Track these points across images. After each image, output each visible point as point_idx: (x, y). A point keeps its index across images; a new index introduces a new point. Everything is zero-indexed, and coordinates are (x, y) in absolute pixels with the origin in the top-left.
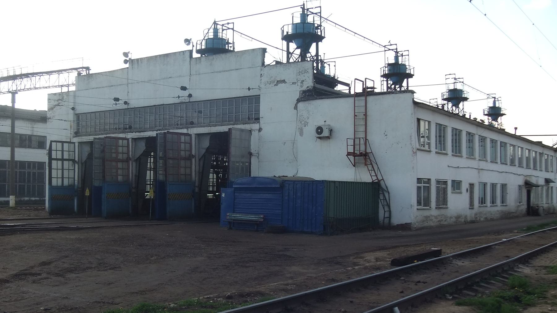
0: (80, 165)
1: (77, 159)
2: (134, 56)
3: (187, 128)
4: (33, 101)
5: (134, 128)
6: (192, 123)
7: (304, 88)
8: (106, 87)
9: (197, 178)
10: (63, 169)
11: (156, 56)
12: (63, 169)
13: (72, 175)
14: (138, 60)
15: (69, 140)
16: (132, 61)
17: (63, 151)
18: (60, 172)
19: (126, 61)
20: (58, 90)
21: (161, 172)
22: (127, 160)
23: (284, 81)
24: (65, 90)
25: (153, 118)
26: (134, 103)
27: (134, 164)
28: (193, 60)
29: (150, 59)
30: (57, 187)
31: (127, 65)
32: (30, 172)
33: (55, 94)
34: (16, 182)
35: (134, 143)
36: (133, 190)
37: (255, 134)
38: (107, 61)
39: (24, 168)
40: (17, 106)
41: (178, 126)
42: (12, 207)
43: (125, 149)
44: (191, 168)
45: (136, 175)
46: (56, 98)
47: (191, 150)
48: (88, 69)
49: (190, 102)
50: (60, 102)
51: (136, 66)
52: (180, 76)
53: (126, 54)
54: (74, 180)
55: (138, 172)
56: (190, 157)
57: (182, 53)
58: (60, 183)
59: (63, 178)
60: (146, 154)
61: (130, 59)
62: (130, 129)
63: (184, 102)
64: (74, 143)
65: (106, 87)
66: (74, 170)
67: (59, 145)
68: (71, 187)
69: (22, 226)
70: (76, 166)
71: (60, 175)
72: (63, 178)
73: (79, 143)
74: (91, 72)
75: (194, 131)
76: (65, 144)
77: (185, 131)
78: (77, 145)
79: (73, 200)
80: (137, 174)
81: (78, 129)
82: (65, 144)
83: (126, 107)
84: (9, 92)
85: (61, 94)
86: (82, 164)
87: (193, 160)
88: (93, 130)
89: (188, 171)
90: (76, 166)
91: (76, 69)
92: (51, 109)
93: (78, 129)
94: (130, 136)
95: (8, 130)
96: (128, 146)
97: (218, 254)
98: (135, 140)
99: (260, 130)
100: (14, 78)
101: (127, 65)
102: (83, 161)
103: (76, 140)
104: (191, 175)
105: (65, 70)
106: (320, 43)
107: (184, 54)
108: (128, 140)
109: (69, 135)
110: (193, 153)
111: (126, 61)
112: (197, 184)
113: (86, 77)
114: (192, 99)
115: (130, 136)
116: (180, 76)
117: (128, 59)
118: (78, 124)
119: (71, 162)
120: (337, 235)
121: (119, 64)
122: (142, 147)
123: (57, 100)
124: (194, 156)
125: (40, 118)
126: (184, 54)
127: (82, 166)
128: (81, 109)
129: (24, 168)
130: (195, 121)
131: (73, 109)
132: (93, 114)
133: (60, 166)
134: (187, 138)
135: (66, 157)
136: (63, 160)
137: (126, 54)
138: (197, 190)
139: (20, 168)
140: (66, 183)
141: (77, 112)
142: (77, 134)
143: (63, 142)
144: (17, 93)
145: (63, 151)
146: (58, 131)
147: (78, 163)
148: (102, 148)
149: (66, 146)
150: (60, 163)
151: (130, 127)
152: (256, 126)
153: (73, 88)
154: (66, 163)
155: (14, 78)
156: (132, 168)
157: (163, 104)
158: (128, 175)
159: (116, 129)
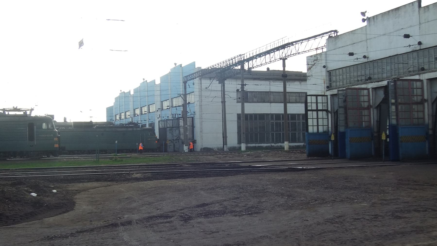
0: (333, 114)
1: (329, 109)
2: (369, 15)
3: (419, 74)
4: (297, 64)
5: (374, 79)
6: (423, 69)
8: (350, 45)
9: (430, 122)
10: (318, 118)
11: (389, 11)
12: (318, 118)
13: (325, 123)
14: (374, 17)
15: (323, 94)
16: (369, 19)
17: (317, 103)
18: (315, 121)
19: (364, 20)
20: (314, 53)
21: (393, 117)
22: (369, 107)
24: (320, 51)
25: (389, 68)
26: (373, 56)
27: (375, 111)
28: (422, 10)
29: (383, 15)
30: (313, 134)
32: (289, 123)
33: (311, 56)
34: (289, 130)
35: (374, 93)
36: (375, 135)
38: (131, 86)
39: (280, 119)
40: (286, 70)
41: (410, 73)
42: (286, 151)
43: (419, 91)
44: (423, 111)
45: (377, 121)
46: (314, 58)
47: (423, 95)
48: (336, 31)
49: (420, 50)
50: (315, 62)
51: (372, 23)
52: (411, 26)
53: (363, 14)
54: (328, 127)
55: (378, 118)
56: (422, 102)
57: (411, 5)
58: (315, 130)
59: (318, 126)
60: (386, 100)
61: (367, 17)
62: (369, 79)
63: (416, 51)
64: (327, 96)
65: (350, 45)
66: (328, 118)
67: (314, 98)
68: (326, 133)
69: (265, 167)
70: (330, 115)
71: (315, 124)
72: (318, 126)
73: (331, 95)
74: (338, 34)
75: (425, 77)
76: (318, 97)
77: (417, 77)
78: (329, 97)
79: (328, 144)
80: (378, 120)
81: (330, 84)
82: (318, 97)
83: (366, 60)
84: (281, 59)
85: (316, 55)
86: (334, 113)
87: (426, 104)
88: (341, 83)
89: (421, 115)
90: (330, 115)
91: (326, 33)
92: (309, 69)
93: (330, 84)
94: (370, 86)
95: (282, 90)
96: (369, 95)
98: (375, 89)
100: (283, 47)
101: (365, 23)
102: (335, 111)
103: (328, 93)
104: (424, 118)
105: (319, 35)
107: (413, 5)
108: (368, 89)
109: (323, 90)
110: (426, 97)
111: (364, 20)
112: (430, 127)
113: (334, 38)
114: (423, 47)
115: (370, 86)
116: (411, 26)
117: (365, 18)
118: (330, 80)
119: (324, 112)
120: (234, 175)
121: (358, 24)
122: (381, 94)
123: (313, 61)
124: (426, 101)
125: (300, 77)
126: (413, 5)
127: (335, 115)
128: (332, 66)
129: (280, 119)
130: (426, 67)
131: (324, 67)
132: (341, 70)
133: (315, 116)
134: (419, 84)
135: (320, 107)
136: (317, 110)
137: (363, 14)
138: (431, 132)
139: (276, 119)
140: (321, 130)
141: (329, 69)
142: (329, 88)
143: (317, 96)
144: (286, 59)
145: (317, 103)
146: (316, 86)
147: (331, 113)
148: (344, 98)
149: (320, 98)
150: (315, 113)
151: (370, 78)
153: (325, 50)
154: (320, 113)
155: (283, 47)
156: (374, 114)
157: (397, 55)
158: (370, 121)
159: (358, 81)
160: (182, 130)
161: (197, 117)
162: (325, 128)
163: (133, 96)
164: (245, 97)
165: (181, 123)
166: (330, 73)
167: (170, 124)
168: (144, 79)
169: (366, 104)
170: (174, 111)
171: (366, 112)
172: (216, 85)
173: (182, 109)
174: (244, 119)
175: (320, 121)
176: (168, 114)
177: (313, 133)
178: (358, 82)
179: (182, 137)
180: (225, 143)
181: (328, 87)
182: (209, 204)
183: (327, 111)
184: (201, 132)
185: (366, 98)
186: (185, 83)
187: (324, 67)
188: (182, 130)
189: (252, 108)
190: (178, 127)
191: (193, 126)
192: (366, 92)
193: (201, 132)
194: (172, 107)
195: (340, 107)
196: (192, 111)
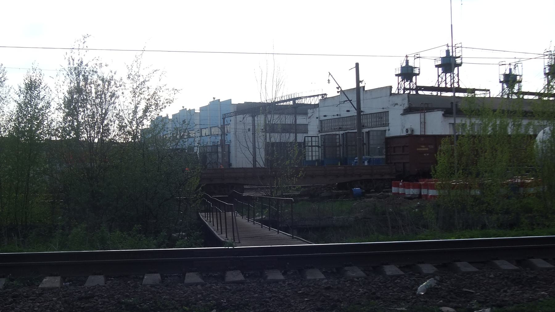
7: (404, 108)
13: (317, 154)
22: (340, 146)
23: (397, 104)
31: (339, 94)
37: (387, 132)
48: (326, 94)
59: (312, 156)
62: (340, 129)
67: (310, 138)
72: (312, 156)
83: (339, 117)
94: (341, 132)
97: (105, 98)
99: (389, 130)
101: (339, 94)
106: (460, 67)
108: (339, 135)
115: (341, 132)
118: (321, 126)
136: (312, 146)
140: (314, 158)
152: (387, 128)
160: (220, 155)
161: (232, 145)
162: (317, 158)
163: (172, 120)
164: (270, 128)
165: (220, 149)
166: (321, 121)
167: (209, 150)
168: (183, 107)
169: (338, 144)
170: (213, 139)
171: (338, 149)
172: (249, 119)
173: (220, 138)
174: (270, 147)
175: (314, 153)
176: (209, 141)
177: (255, 168)
178: (335, 130)
179: (220, 161)
180: (254, 164)
181: (319, 131)
182: (254, 123)
183: (318, 146)
184: (236, 156)
185: (338, 141)
186: (224, 119)
187: (317, 118)
188: (220, 155)
189: (276, 138)
190: (217, 152)
191: (229, 152)
192: (338, 136)
193: (236, 156)
194: (211, 135)
195: (475, 95)
196: (229, 140)
